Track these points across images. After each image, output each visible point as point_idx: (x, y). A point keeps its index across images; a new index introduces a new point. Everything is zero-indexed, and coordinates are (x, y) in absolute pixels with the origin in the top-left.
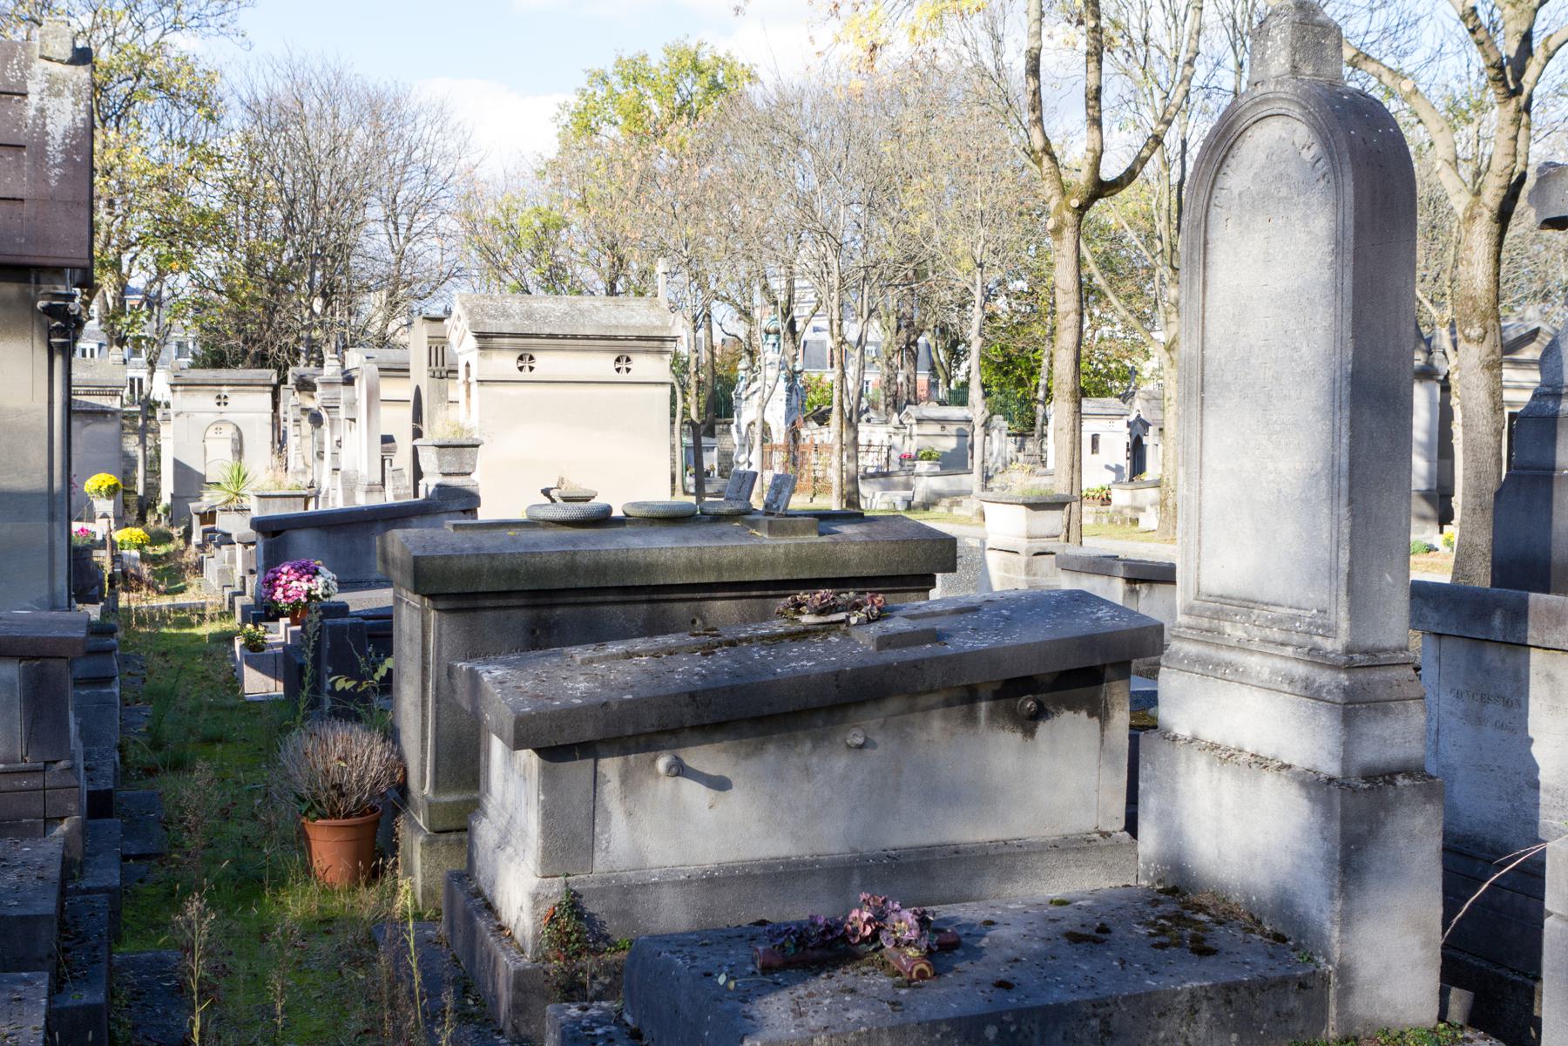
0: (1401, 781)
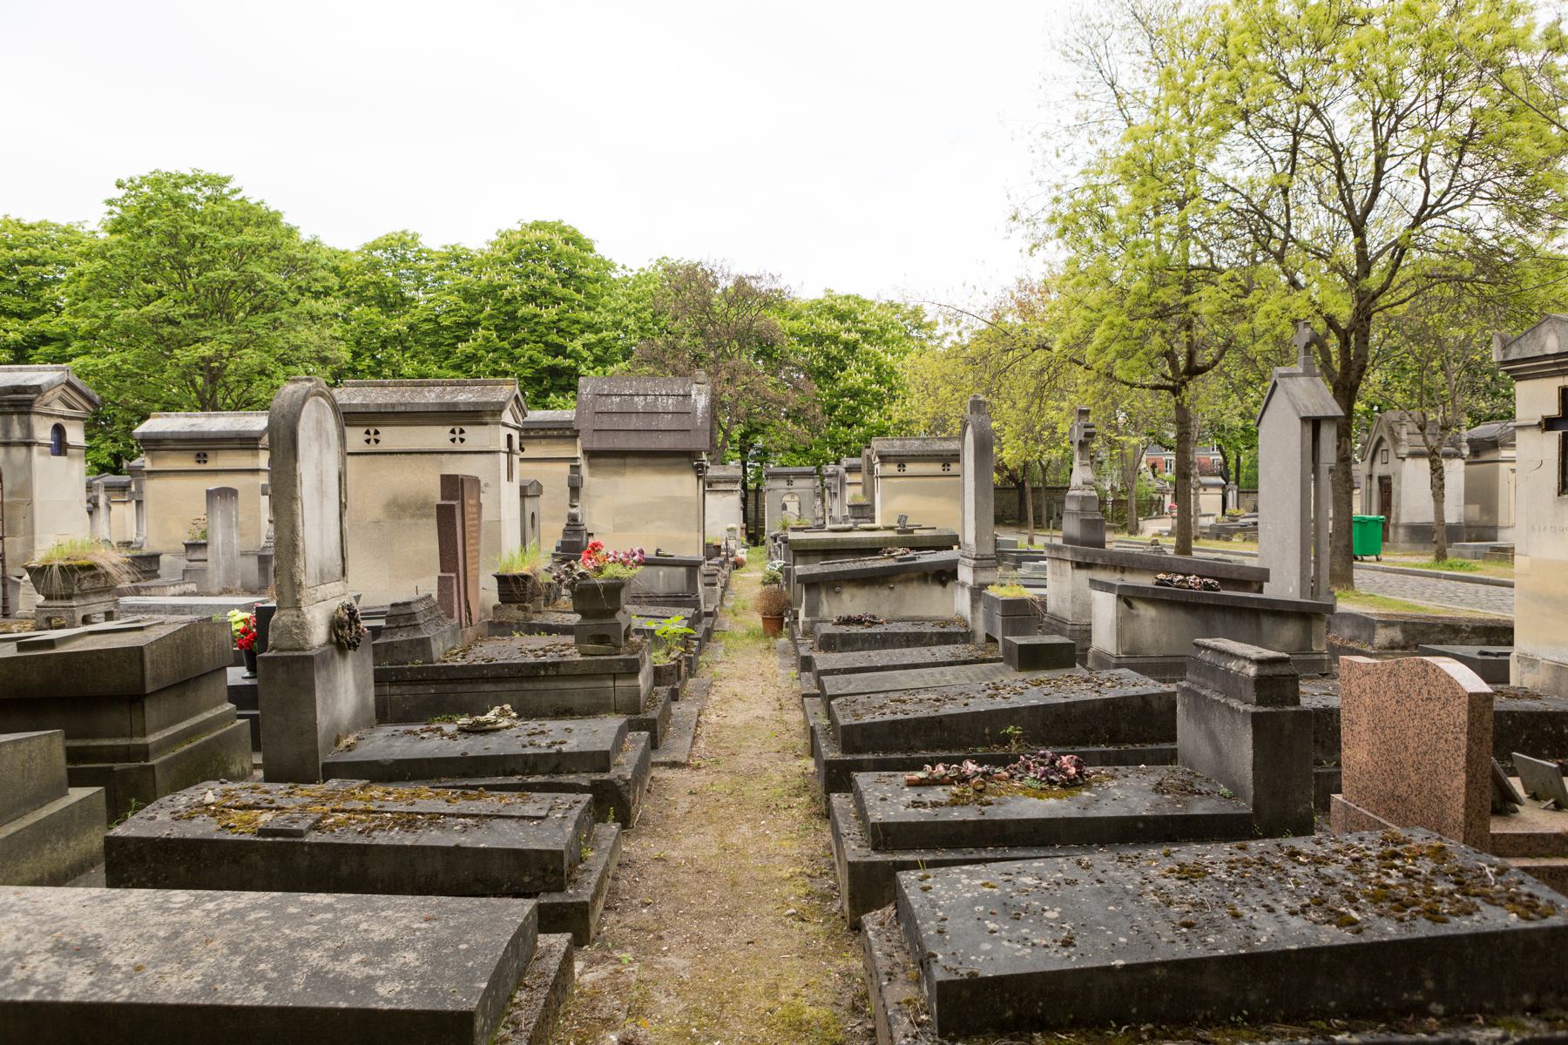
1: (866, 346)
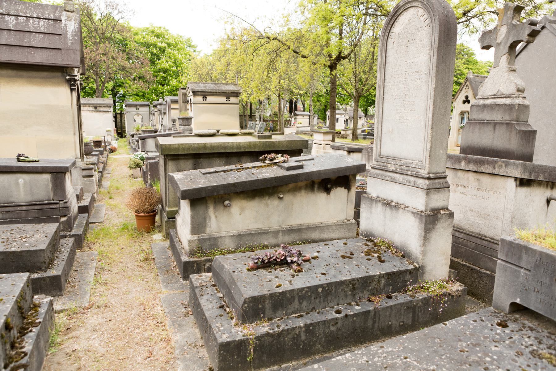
0: (442, 212)
1: (169, 50)
